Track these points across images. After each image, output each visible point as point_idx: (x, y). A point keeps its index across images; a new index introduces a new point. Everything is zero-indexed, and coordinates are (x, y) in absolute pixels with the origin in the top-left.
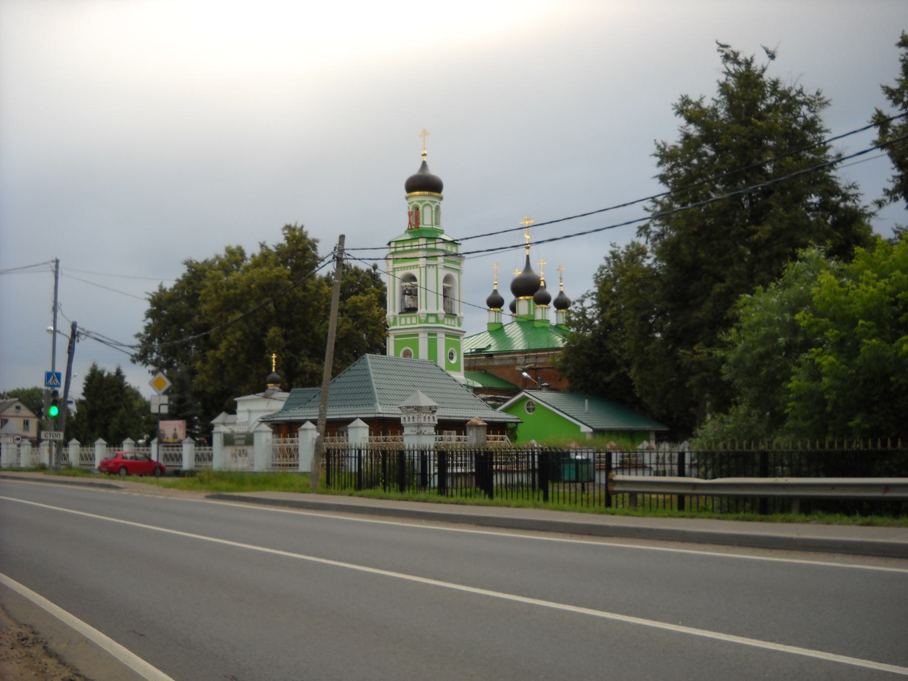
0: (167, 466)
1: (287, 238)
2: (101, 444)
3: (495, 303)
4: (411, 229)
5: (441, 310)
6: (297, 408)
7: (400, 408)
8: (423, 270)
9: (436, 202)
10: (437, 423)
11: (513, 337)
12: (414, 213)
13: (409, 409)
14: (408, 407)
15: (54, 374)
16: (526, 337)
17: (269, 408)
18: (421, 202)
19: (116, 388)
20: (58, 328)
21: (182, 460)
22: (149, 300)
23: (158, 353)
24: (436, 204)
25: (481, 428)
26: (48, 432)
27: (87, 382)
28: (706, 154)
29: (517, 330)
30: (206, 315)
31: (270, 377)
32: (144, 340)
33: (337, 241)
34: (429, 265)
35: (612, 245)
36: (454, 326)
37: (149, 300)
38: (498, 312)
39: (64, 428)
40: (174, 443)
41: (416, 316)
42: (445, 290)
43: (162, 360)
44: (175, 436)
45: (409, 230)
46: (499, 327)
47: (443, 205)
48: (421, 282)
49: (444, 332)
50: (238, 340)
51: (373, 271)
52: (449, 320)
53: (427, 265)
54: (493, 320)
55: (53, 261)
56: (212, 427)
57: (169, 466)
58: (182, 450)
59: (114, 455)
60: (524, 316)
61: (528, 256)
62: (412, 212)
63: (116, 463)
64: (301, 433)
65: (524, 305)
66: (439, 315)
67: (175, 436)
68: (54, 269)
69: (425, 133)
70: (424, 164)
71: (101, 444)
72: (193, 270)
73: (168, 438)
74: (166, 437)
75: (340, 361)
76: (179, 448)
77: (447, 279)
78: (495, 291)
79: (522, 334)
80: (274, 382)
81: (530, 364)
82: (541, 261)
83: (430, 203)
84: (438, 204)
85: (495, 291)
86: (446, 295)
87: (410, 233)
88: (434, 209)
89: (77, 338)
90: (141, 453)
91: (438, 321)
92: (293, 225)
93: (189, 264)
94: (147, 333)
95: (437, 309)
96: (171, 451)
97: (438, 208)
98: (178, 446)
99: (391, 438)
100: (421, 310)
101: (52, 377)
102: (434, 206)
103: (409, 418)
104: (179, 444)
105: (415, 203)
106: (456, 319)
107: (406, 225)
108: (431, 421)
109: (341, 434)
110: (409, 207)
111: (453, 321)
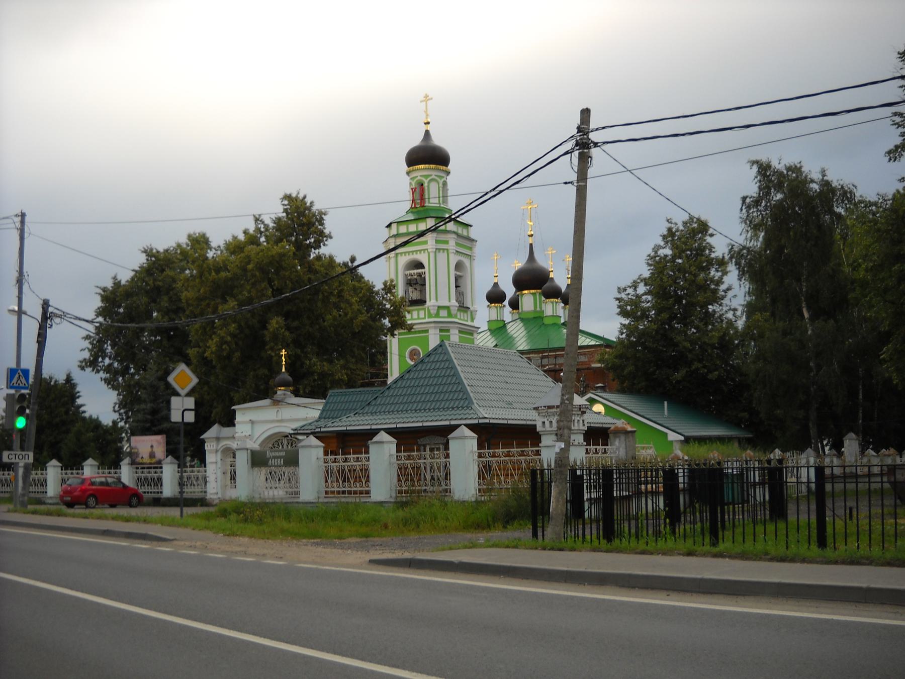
0: (145, 492)
1: (285, 211)
2: (54, 466)
3: (496, 297)
4: (415, 207)
5: (454, 302)
6: (352, 415)
7: (536, 409)
8: (432, 255)
9: (443, 177)
10: (586, 429)
11: (515, 336)
12: (418, 190)
13: (549, 410)
14: (549, 407)
15: (19, 371)
16: (530, 337)
17: (280, 418)
18: (426, 176)
19: (66, 399)
20: (24, 308)
21: (161, 485)
22: (100, 294)
23: (110, 358)
24: (443, 180)
25: (630, 434)
26: (12, 452)
27: (72, 382)
28: (245, 295)
29: (521, 331)
30: (188, 305)
31: (279, 378)
32: (95, 342)
33: (577, 120)
34: (439, 249)
35: (668, 221)
36: (467, 321)
37: (100, 294)
38: (500, 307)
39: (33, 449)
40: (151, 464)
41: (424, 309)
42: (457, 278)
43: (116, 365)
44: (152, 455)
45: (412, 210)
46: (501, 325)
47: (450, 179)
48: (429, 273)
49: (457, 327)
50: (233, 336)
51: (350, 264)
52: (462, 314)
53: (436, 249)
54: (494, 317)
55: (16, 216)
56: (203, 442)
57: (148, 493)
58: (47, 474)
59: (79, 481)
60: (528, 312)
61: (531, 245)
62: (416, 188)
63: (84, 491)
64: (372, 448)
65: (528, 300)
66: (451, 308)
67: (152, 455)
68: (18, 225)
69: (427, 98)
70: (427, 134)
71: (54, 466)
72: (153, 259)
73: (142, 458)
74: (140, 456)
75: (354, 360)
76: (158, 470)
77: (459, 266)
78: (496, 284)
79: (524, 333)
80: (285, 384)
81: (551, 365)
82: (550, 249)
83: (436, 178)
84: (444, 179)
85: (496, 284)
86: (458, 284)
87: (412, 212)
88: (441, 185)
89: (49, 322)
90: (114, 477)
91: (450, 315)
92: (294, 195)
93: (148, 252)
94: (97, 334)
95: (450, 301)
96: (146, 474)
97: (445, 184)
98: (157, 468)
99: (517, 452)
100: (431, 302)
101: (17, 376)
102: (441, 182)
103: (551, 422)
104: (158, 465)
105: (419, 178)
106: (469, 313)
107: (408, 205)
108: (582, 427)
109: (422, 448)
110: (411, 184)
111: (465, 315)
